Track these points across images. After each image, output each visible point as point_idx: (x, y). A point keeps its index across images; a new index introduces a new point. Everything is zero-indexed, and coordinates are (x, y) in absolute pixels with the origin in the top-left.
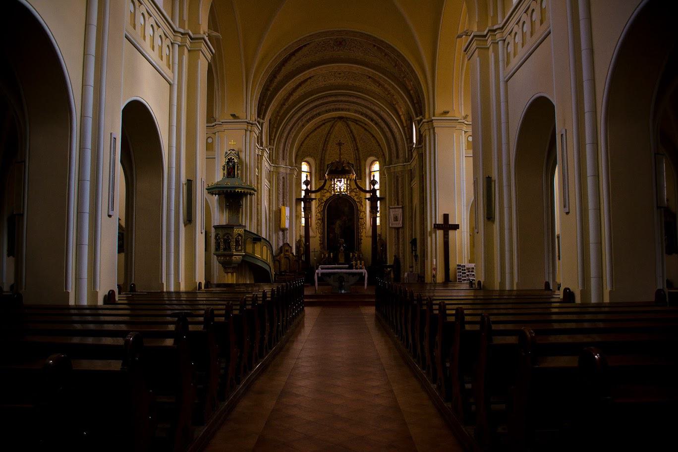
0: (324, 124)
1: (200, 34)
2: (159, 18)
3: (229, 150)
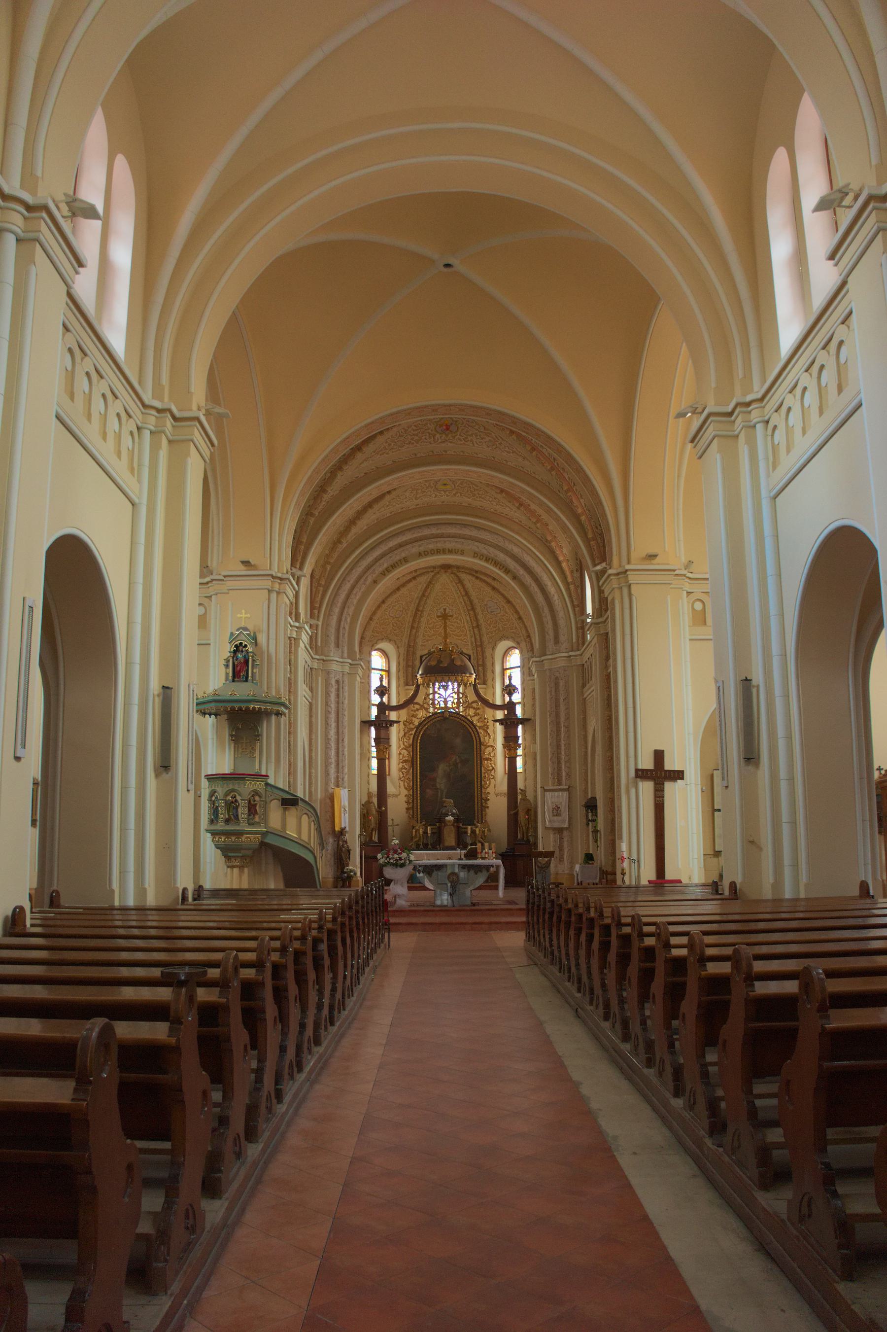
0: (414, 578)
1: (191, 410)
2: (115, 380)
3: (238, 630)
